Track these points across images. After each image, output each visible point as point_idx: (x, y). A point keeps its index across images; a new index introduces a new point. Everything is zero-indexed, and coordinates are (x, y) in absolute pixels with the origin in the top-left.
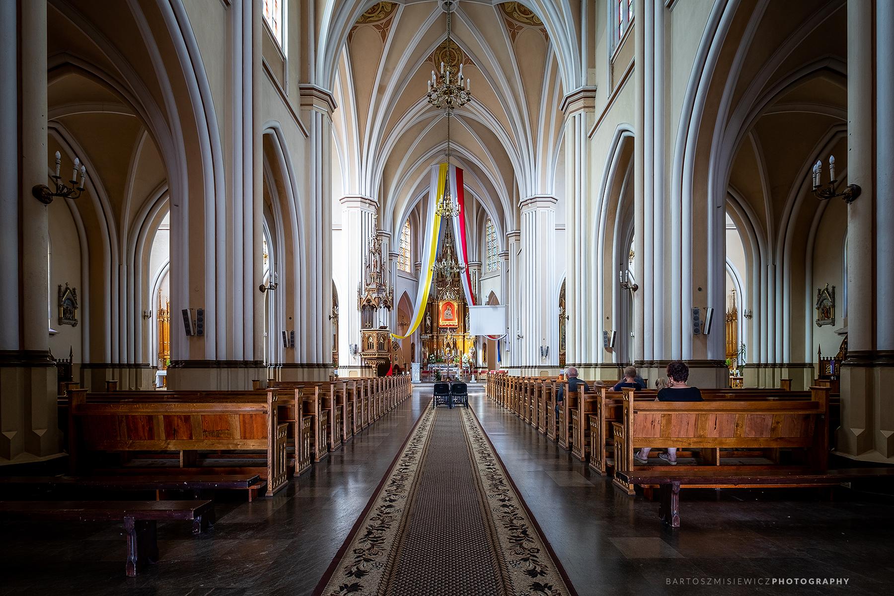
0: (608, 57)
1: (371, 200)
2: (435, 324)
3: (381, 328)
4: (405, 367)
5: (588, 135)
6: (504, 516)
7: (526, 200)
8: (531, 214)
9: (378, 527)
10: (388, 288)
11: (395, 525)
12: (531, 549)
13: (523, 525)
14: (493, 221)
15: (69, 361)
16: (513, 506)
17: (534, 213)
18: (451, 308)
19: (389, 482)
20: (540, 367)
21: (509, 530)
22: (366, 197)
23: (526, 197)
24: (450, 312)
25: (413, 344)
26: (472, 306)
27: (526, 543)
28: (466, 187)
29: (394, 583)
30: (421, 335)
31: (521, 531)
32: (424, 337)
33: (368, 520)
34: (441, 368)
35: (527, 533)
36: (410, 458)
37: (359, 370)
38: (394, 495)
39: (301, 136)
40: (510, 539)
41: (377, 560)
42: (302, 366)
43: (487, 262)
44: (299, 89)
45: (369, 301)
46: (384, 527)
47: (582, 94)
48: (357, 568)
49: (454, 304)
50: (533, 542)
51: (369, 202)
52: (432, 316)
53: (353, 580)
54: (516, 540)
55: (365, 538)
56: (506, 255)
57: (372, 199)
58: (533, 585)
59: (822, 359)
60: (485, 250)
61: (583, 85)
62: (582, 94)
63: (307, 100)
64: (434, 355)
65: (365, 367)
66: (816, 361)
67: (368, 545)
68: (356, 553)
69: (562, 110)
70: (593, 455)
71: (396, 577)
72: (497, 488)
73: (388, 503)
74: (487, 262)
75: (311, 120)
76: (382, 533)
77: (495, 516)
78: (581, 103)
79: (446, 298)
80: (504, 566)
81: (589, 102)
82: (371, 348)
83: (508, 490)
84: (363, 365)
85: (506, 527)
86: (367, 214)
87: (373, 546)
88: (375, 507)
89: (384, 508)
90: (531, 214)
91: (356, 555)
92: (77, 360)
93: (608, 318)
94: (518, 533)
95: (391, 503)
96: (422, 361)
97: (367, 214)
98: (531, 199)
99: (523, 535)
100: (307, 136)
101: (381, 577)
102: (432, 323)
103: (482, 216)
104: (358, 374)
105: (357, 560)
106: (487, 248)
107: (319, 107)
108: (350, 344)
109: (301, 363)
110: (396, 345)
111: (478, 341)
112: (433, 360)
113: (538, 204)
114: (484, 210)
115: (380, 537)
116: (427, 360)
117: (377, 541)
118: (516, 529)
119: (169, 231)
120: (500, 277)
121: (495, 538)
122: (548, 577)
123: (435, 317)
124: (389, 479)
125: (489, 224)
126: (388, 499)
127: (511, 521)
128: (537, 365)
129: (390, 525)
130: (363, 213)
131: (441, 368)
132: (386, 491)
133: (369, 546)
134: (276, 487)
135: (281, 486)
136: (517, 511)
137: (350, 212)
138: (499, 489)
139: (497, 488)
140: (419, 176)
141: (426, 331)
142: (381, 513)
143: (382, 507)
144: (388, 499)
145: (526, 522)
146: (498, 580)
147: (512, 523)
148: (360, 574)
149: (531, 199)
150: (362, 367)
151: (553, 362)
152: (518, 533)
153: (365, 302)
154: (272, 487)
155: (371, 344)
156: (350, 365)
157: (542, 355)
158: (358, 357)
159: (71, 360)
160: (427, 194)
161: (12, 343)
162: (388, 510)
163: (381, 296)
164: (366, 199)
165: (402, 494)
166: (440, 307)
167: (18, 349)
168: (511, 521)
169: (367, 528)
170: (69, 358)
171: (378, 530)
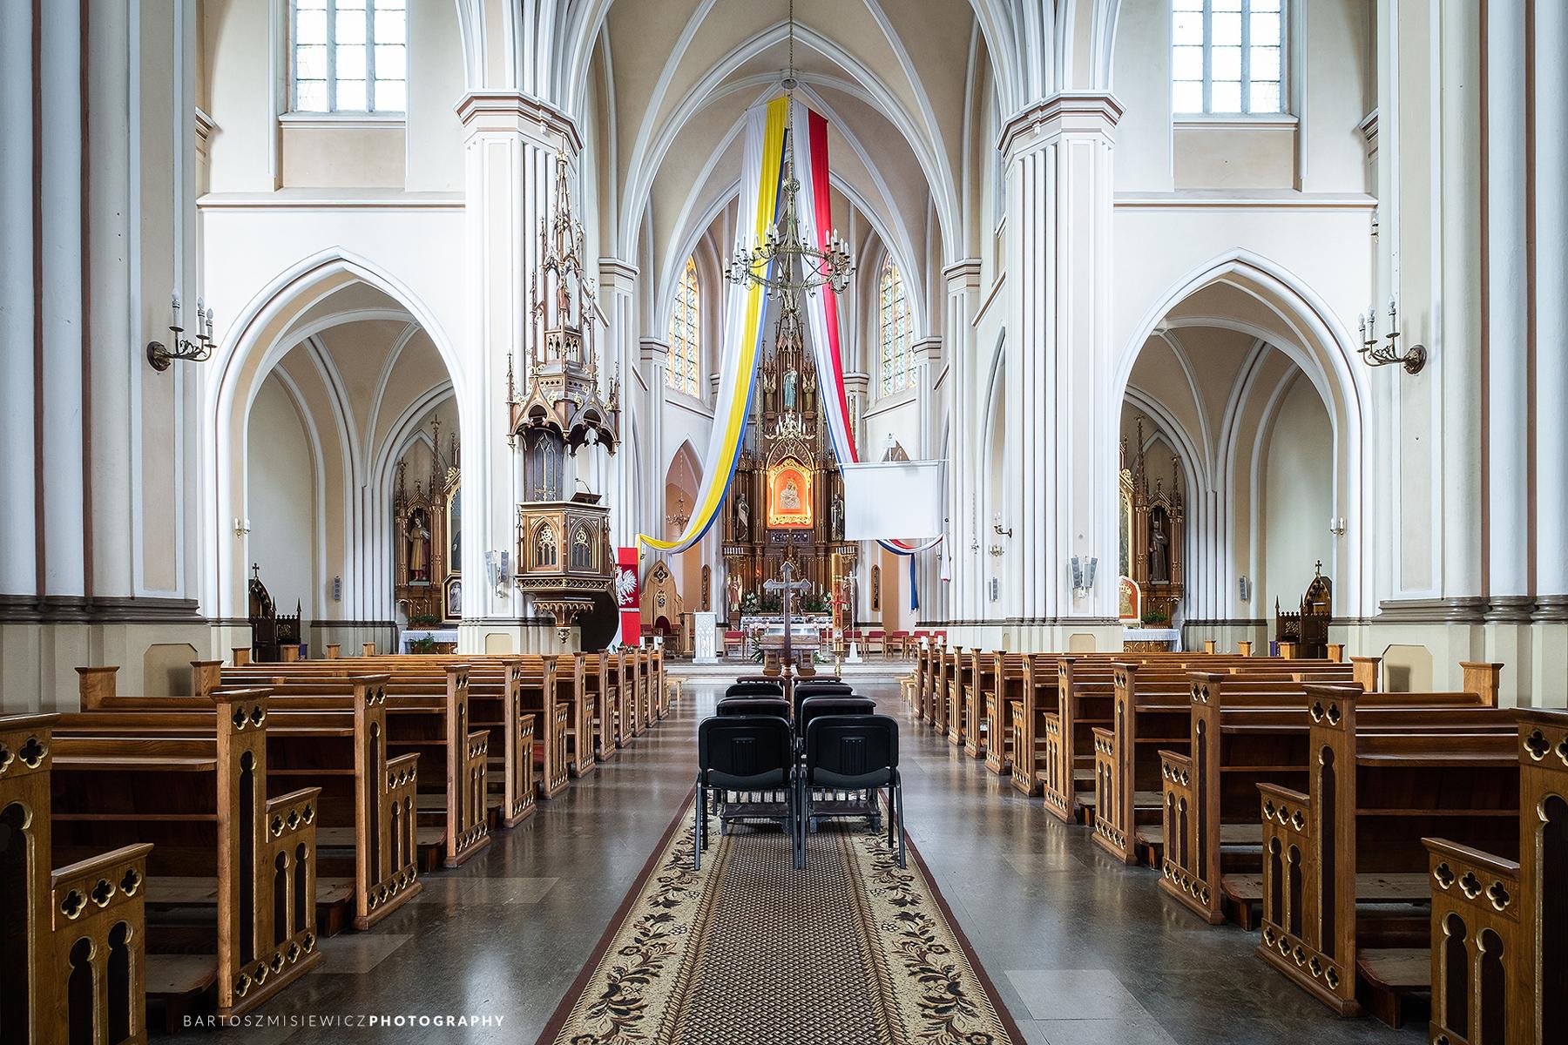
0: (992, 229)
1: (553, 114)
2: (758, 522)
3: (579, 497)
4: (683, 623)
5: (973, 323)
6: (904, 944)
7: (1026, 115)
8: (1040, 155)
9: (635, 973)
10: (601, 371)
11: (671, 966)
12: (973, 1034)
13: (949, 968)
14: (901, 265)
15: (296, 618)
16: (922, 918)
17: (1051, 150)
18: (797, 483)
19: (667, 858)
20: (1069, 622)
21: (920, 980)
22: (537, 100)
23: (1027, 102)
25: (706, 569)
26: (853, 465)
27: (959, 1019)
28: (837, 182)
29: (688, 1019)
30: (724, 547)
31: (946, 983)
32: (730, 551)
33: (674, 843)
34: (772, 626)
35: (960, 989)
36: (686, 869)
37: (516, 632)
38: (675, 889)
40: (925, 1007)
41: (690, 889)
42: (355, 624)
43: (883, 375)
45: (538, 412)
46: (645, 972)
47: (964, 270)
48: (665, 898)
49: (804, 474)
50: (974, 1015)
51: (548, 117)
52: (751, 503)
53: (661, 910)
54: (938, 1011)
55: (601, 1004)
56: (935, 345)
57: (556, 107)
58: (900, 915)
59: (1281, 615)
62: (964, 270)
63: (647, 354)
65: (537, 622)
66: (1271, 616)
67: (677, 872)
68: (661, 882)
69: (1000, 148)
70: (1102, 815)
71: (693, 1002)
72: (889, 873)
73: (661, 910)
76: (640, 989)
77: (887, 945)
78: (964, 279)
79: (783, 430)
80: (897, 1024)
81: (935, 353)
82: (547, 563)
83: (912, 878)
84: (530, 614)
85: (913, 974)
86: (540, 156)
87: (683, 874)
88: (633, 921)
89: (652, 921)
90: (1040, 155)
91: (661, 884)
92: (306, 617)
93: (1081, 536)
94: (939, 989)
95: (667, 910)
96: (727, 607)
97: (540, 156)
98: (1042, 108)
99: (949, 996)
100: (607, 326)
101: (666, 1002)
102: (751, 518)
103: (872, 249)
104: (512, 643)
105: (663, 889)
108: (489, 550)
109: (37, 598)
110: (661, 568)
111: (859, 561)
112: (754, 605)
113: (1066, 121)
114: (877, 240)
115: (636, 1001)
116: (740, 605)
117: (626, 1013)
118: (936, 979)
120: (914, 406)
121: (890, 1004)
122: (921, 906)
123: (759, 503)
124: (669, 852)
125: (888, 281)
126: (661, 899)
127: (922, 955)
128: (1060, 615)
129: (661, 967)
130: (529, 149)
131: (772, 626)
132: (659, 880)
133: (609, 1026)
134: (380, 905)
135: (376, 914)
136: (932, 931)
137: (486, 142)
138: (893, 876)
139: (889, 873)
140: (716, 145)
142: (645, 935)
143: (647, 919)
144: (661, 899)
145: (955, 959)
146: (868, 974)
147: (924, 961)
148: (669, 904)
149: (1042, 108)
150: (524, 621)
152: (939, 989)
153: (526, 414)
154: (457, 851)
155: (547, 550)
156: (490, 615)
157: (1077, 584)
158: (515, 593)
159: (299, 616)
160: (733, 204)
161: (23, 585)
162: (660, 928)
163: (576, 397)
164: (538, 108)
165: (692, 888)
167: (35, 594)
168: (922, 955)
169: (609, 977)
171: (632, 981)
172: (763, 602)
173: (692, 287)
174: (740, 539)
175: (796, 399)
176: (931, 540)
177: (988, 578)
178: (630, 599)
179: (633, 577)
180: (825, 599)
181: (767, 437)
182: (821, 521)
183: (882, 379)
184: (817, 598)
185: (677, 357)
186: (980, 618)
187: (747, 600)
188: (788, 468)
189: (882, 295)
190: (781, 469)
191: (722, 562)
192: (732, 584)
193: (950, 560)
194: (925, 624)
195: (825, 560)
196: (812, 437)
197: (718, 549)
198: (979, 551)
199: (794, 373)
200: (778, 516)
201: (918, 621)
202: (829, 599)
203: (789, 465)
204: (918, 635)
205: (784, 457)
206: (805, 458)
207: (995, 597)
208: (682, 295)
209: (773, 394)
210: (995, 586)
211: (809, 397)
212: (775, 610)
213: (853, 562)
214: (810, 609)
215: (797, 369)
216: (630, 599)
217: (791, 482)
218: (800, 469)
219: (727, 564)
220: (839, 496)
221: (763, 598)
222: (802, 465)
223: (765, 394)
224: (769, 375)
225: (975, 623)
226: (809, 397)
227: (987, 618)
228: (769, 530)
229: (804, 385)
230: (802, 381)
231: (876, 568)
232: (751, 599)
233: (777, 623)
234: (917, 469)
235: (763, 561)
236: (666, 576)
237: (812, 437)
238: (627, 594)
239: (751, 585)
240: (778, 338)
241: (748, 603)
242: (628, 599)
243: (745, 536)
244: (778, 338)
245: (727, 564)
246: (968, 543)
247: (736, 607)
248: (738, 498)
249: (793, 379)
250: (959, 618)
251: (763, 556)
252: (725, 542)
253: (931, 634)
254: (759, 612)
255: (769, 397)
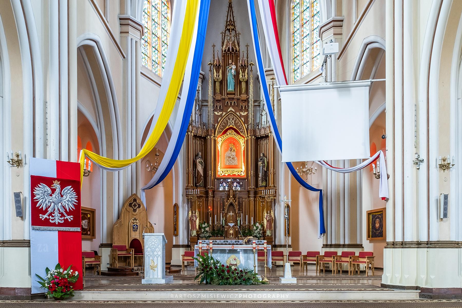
2: (210, 173)
18: (236, 147)
24: (234, 154)
25: (176, 206)
32: (191, 192)
39: (121, 58)
44: (119, 19)
60: (289, 47)
61: (333, 16)
63: (125, 28)
64: (208, 223)
74: (292, 67)
75: (127, 45)
78: (332, 31)
81: (338, 30)
100: (124, 57)
106: (292, 44)
107: (133, 34)
110: (135, 200)
111: (277, 201)
112: (207, 232)
116: (197, 232)
119: (67, 161)
141: (196, 184)
151: (459, 250)
166: (219, 146)
170: (418, 293)
172: (214, 230)
173: (166, 3)
174: (198, 185)
175: (235, 86)
176: (364, 160)
177: (434, 195)
178: (70, 218)
179: (74, 194)
180: (255, 228)
181: (216, 113)
182: (252, 173)
183: (292, 71)
184: (249, 226)
185: (154, 49)
186: (424, 238)
187: (202, 228)
188: (229, 136)
189: (292, 11)
190: (225, 137)
191: (186, 201)
192: (192, 216)
193: (388, 178)
194: (331, 246)
195: (254, 200)
196: (246, 113)
197: (183, 193)
198: (423, 166)
199: (234, 67)
200: (223, 170)
201: (325, 243)
202: (257, 227)
203: (231, 134)
204: (328, 254)
205: (227, 127)
206: (241, 129)
207: (445, 215)
208: (158, 5)
209: (220, 82)
210: (446, 203)
211: (244, 85)
212: (221, 236)
213: (273, 201)
214: (245, 235)
215: (236, 65)
216: (70, 218)
217: (231, 146)
218: (237, 137)
219: (189, 202)
220: (264, 155)
221: (213, 227)
222: (239, 134)
223: (215, 82)
224: (218, 67)
225: (419, 244)
226: (244, 85)
227: (434, 238)
228: (217, 179)
229: (241, 76)
230: (239, 74)
231: (288, 206)
232: (205, 228)
233: (222, 244)
234: (349, 90)
235: (213, 201)
236: (139, 206)
237: (246, 113)
238: (66, 211)
239: (205, 218)
240: (223, 43)
241: (203, 230)
242: (68, 217)
243: (201, 182)
244: (223, 43)
245: (189, 202)
246: (410, 158)
247: (194, 233)
248: (197, 155)
249: (233, 71)
250: (399, 239)
251: (214, 197)
252: (188, 186)
253: (338, 254)
254: (210, 237)
255: (217, 84)
